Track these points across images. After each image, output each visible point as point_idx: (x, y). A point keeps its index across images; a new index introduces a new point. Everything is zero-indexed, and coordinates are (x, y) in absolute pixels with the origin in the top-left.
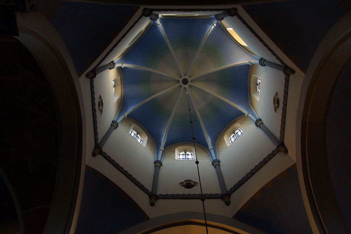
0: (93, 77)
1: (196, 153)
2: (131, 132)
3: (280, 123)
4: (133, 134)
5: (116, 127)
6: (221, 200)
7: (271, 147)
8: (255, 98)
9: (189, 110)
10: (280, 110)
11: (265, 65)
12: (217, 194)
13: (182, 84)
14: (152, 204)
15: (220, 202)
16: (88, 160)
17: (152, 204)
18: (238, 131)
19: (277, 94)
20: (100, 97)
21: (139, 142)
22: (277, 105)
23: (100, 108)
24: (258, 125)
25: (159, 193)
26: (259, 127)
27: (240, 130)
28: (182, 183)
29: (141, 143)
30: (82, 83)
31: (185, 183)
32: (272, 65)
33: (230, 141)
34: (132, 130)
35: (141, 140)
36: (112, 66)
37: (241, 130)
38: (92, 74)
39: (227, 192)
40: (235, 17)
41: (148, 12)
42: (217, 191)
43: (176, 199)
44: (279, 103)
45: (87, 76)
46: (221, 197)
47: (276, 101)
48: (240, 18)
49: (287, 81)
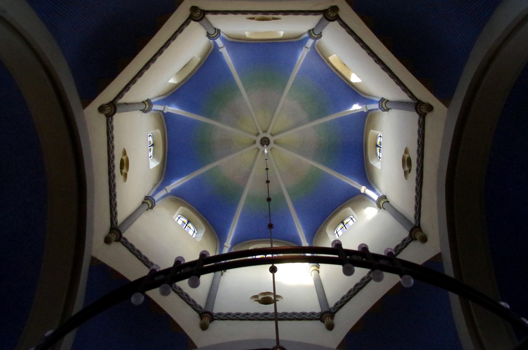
0: (112, 112)
1: (268, 207)
2: (177, 218)
3: (414, 194)
4: (180, 222)
5: (150, 206)
6: (319, 322)
7: (414, 117)
8: (372, 166)
9: (268, 182)
10: (413, 174)
11: (388, 110)
12: (313, 313)
13: (260, 147)
14: (204, 327)
15: (318, 326)
16: (97, 247)
17: (204, 327)
18: (348, 220)
19: (406, 151)
20: (125, 153)
21: (191, 234)
22: (407, 169)
23: (124, 171)
24: (381, 204)
25: (216, 310)
26: (382, 209)
27: (352, 219)
28: (256, 297)
29: (194, 236)
30: (91, 119)
31: (260, 298)
32: (400, 105)
33: (336, 235)
34: (179, 216)
35: (194, 232)
36: (147, 106)
37: (353, 219)
38: (109, 108)
39: (330, 309)
40: (336, 23)
41: (199, 13)
42: (317, 309)
43: (245, 320)
44: (413, 164)
45: (101, 109)
46: (319, 317)
47: (407, 162)
48: (344, 25)
49: (422, 125)
